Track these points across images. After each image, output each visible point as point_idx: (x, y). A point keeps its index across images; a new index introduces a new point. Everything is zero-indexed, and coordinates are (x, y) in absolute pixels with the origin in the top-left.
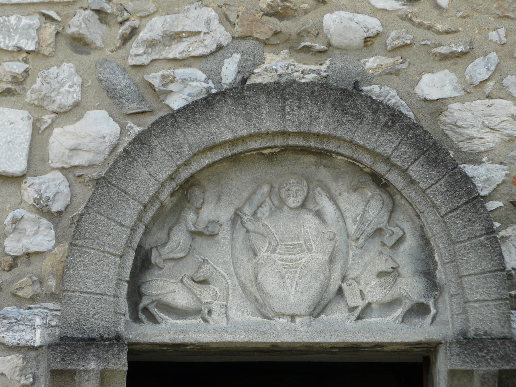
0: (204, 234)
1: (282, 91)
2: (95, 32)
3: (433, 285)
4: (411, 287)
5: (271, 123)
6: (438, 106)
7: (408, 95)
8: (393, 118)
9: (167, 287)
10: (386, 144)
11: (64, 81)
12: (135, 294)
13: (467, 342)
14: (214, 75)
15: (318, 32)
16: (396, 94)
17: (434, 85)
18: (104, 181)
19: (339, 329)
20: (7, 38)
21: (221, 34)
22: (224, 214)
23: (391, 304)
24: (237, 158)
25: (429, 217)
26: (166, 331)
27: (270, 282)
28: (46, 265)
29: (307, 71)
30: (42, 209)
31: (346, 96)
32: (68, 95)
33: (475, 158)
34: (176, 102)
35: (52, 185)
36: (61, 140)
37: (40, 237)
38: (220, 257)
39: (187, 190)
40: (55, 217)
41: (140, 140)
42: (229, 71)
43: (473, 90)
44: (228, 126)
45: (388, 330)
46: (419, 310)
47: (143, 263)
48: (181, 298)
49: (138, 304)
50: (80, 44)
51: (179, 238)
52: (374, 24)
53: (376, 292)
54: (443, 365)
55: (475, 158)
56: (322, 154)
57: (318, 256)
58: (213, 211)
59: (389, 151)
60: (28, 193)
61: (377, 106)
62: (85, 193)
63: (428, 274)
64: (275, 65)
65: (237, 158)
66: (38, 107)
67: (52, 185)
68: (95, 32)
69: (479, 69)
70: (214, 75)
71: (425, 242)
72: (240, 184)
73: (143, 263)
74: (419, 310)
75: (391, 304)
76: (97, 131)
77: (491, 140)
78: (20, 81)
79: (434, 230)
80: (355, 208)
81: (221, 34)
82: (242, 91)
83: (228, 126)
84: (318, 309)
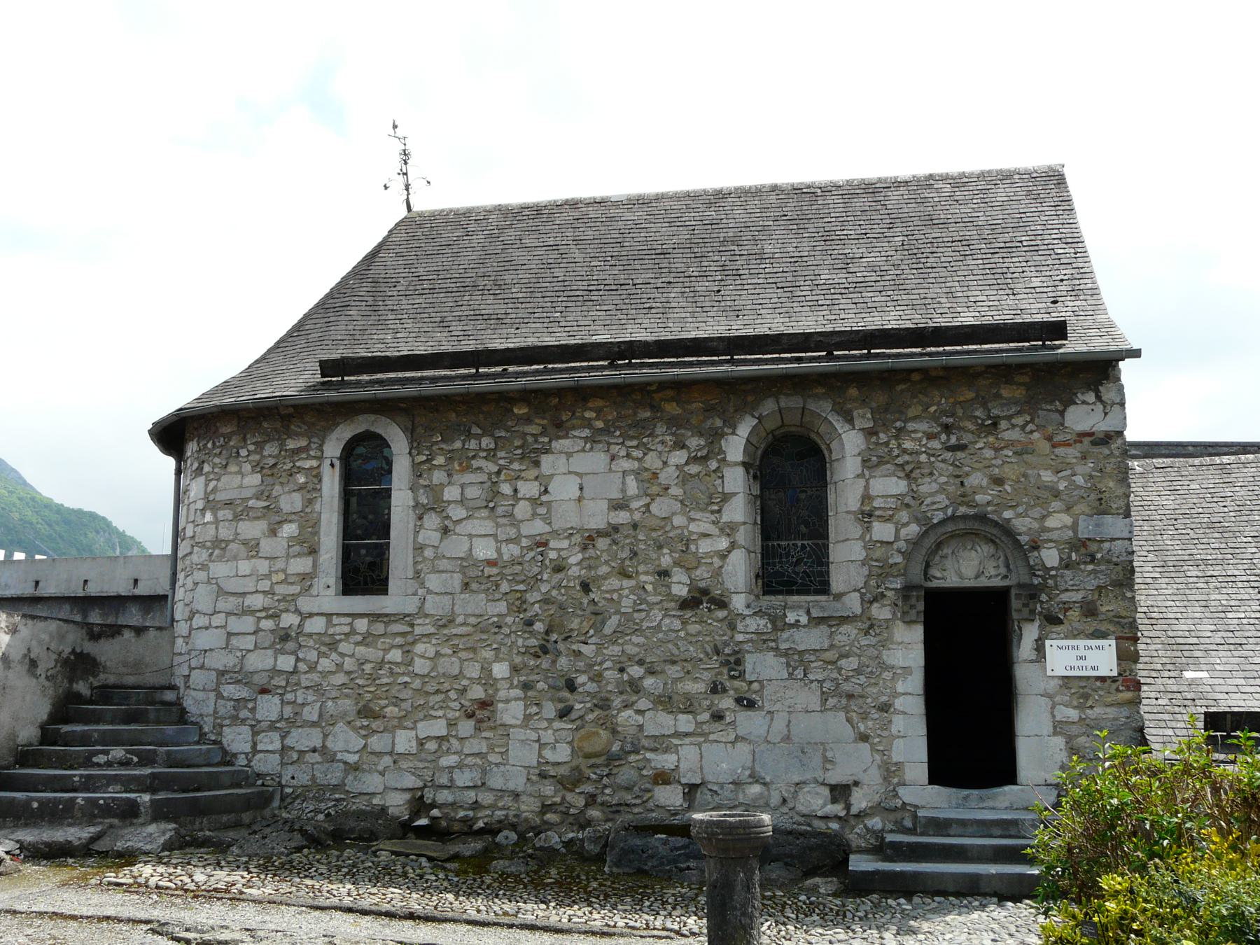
0: (945, 557)
1: (965, 517)
2: (912, 503)
3: (1009, 570)
4: (1003, 570)
5: (962, 526)
6: (1009, 520)
7: (1000, 517)
8: (996, 523)
9: (935, 572)
10: (995, 531)
11: (904, 516)
12: (926, 573)
13: (1020, 586)
14: (945, 513)
15: (974, 501)
16: (750, 661)
17: (1007, 514)
18: (916, 543)
19: (983, 582)
20: (1065, 597)
21: (947, 502)
22: (950, 552)
23: (997, 576)
24: (953, 536)
25: (1008, 551)
26: (935, 584)
27: (963, 570)
28: (901, 566)
29: (971, 512)
30: (899, 551)
31: (982, 518)
32: (905, 520)
33: (1020, 534)
34: (935, 521)
35: (902, 545)
36: (903, 532)
37: (899, 559)
38: (948, 563)
39: (939, 545)
40: (903, 553)
41: (926, 532)
42: (950, 512)
43: (1019, 515)
44: (950, 528)
45: (997, 582)
46: (1006, 577)
47: (928, 566)
48: (938, 575)
49: (927, 577)
50: (908, 506)
51: (937, 558)
52: (990, 498)
53: (993, 572)
54: (1013, 592)
55: (1020, 534)
56: (976, 534)
57: (976, 562)
58: (947, 551)
59: (271, 661)
60: (895, 546)
61: (992, 521)
62: (911, 547)
63: (1008, 566)
64: (962, 510)
65: (953, 536)
66: (896, 523)
67: (902, 545)
68: (912, 503)
69: (1020, 510)
70: (945, 513)
71: (1006, 558)
72: (953, 543)
73: (928, 566)
74: (1006, 577)
75: (997, 576)
76: (913, 529)
77: (1024, 529)
78: (892, 516)
79: (1009, 555)
80: (985, 549)
81: (947, 502)
82: (953, 518)
83: (950, 528)
84: (977, 577)
